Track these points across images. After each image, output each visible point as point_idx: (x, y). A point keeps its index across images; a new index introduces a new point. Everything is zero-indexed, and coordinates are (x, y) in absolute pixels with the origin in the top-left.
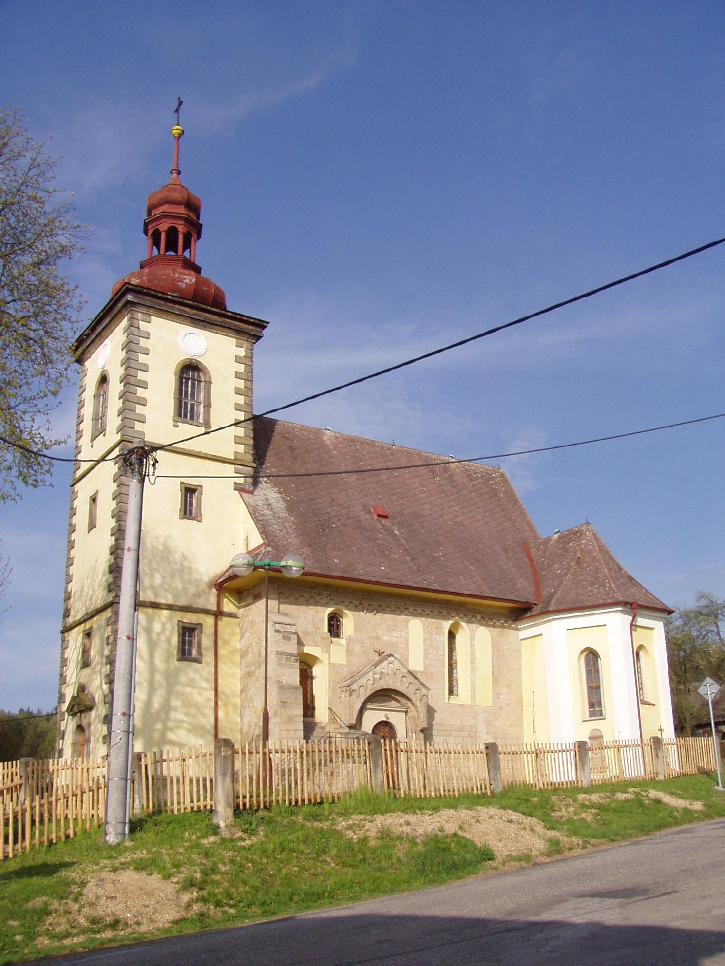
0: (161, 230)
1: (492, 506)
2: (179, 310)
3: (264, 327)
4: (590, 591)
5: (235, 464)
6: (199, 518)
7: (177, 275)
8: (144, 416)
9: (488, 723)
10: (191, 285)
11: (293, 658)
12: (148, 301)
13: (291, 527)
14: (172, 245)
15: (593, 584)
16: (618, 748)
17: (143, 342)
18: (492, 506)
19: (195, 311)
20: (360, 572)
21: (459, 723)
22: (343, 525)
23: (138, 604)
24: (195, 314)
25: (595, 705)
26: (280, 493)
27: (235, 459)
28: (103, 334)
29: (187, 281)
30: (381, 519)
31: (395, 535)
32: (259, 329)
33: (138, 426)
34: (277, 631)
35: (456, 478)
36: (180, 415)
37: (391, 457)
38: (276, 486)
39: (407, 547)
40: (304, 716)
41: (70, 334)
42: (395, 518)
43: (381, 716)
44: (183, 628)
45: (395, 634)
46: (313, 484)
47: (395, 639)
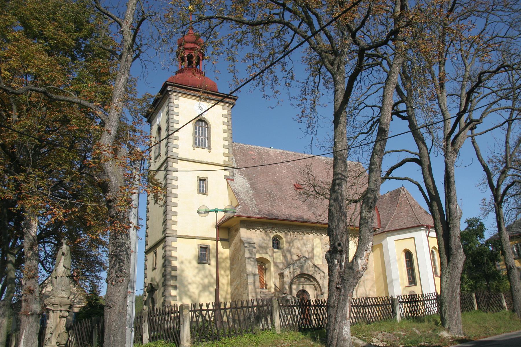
3: (236, 100)
8: (178, 145)
12: (178, 89)
14: (190, 63)
17: (176, 110)
23: (460, 96)
33: (175, 150)
41: (291, 338)
44: (201, 247)
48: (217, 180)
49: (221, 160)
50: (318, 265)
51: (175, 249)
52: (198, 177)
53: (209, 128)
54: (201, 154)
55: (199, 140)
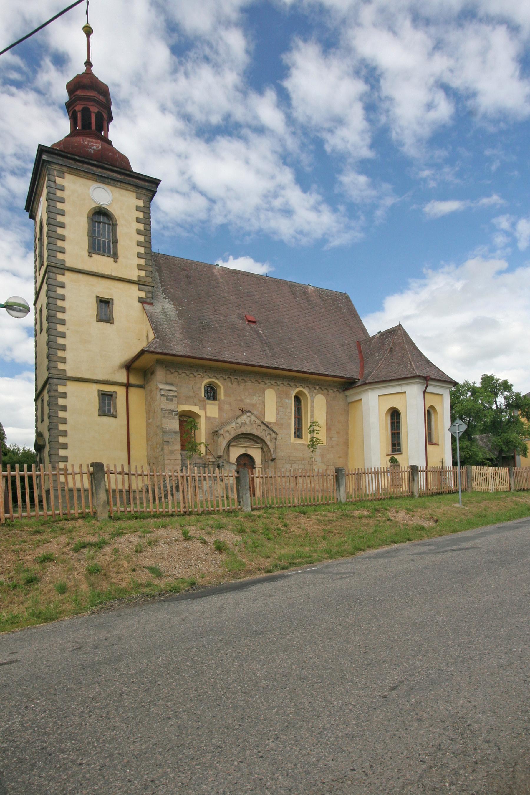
0: (77, 110)
1: (337, 317)
2: (87, 168)
4: (396, 370)
5: (138, 284)
6: (112, 321)
7: (86, 143)
8: (64, 248)
9: (322, 456)
10: (98, 151)
11: (173, 413)
12: (60, 160)
13: (178, 327)
15: (399, 364)
16: (377, 473)
18: (337, 317)
19: (100, 170)
20: (227, 356)
21: (301, 455)
22: (220, 327)
24: (100, 172)
25: (396, 444)
26: (175, 305)
27: (139, 281)
28: (38, 192)
29: (95, 147)
30: (250, 324)
31: (260, 334)
32: (154, 186)
34: (162, 395)
35: (312, 299)
36: (94, 249)
37: (264, 284)
38: (172, 300)
39: (267, 341)
40: (182, 449)
42: (262, 323)
43: (242, 451)
44: (102, 394)
45: (255, 398)
46: (202, 300)
47: (255, 402)
48: (127, 301)
49: (134, 274)
50: (270, 423)
51: (64, 395)
52: (97, 297)
53: (115, 226)
54: (101, 263)
55: (99, 244)
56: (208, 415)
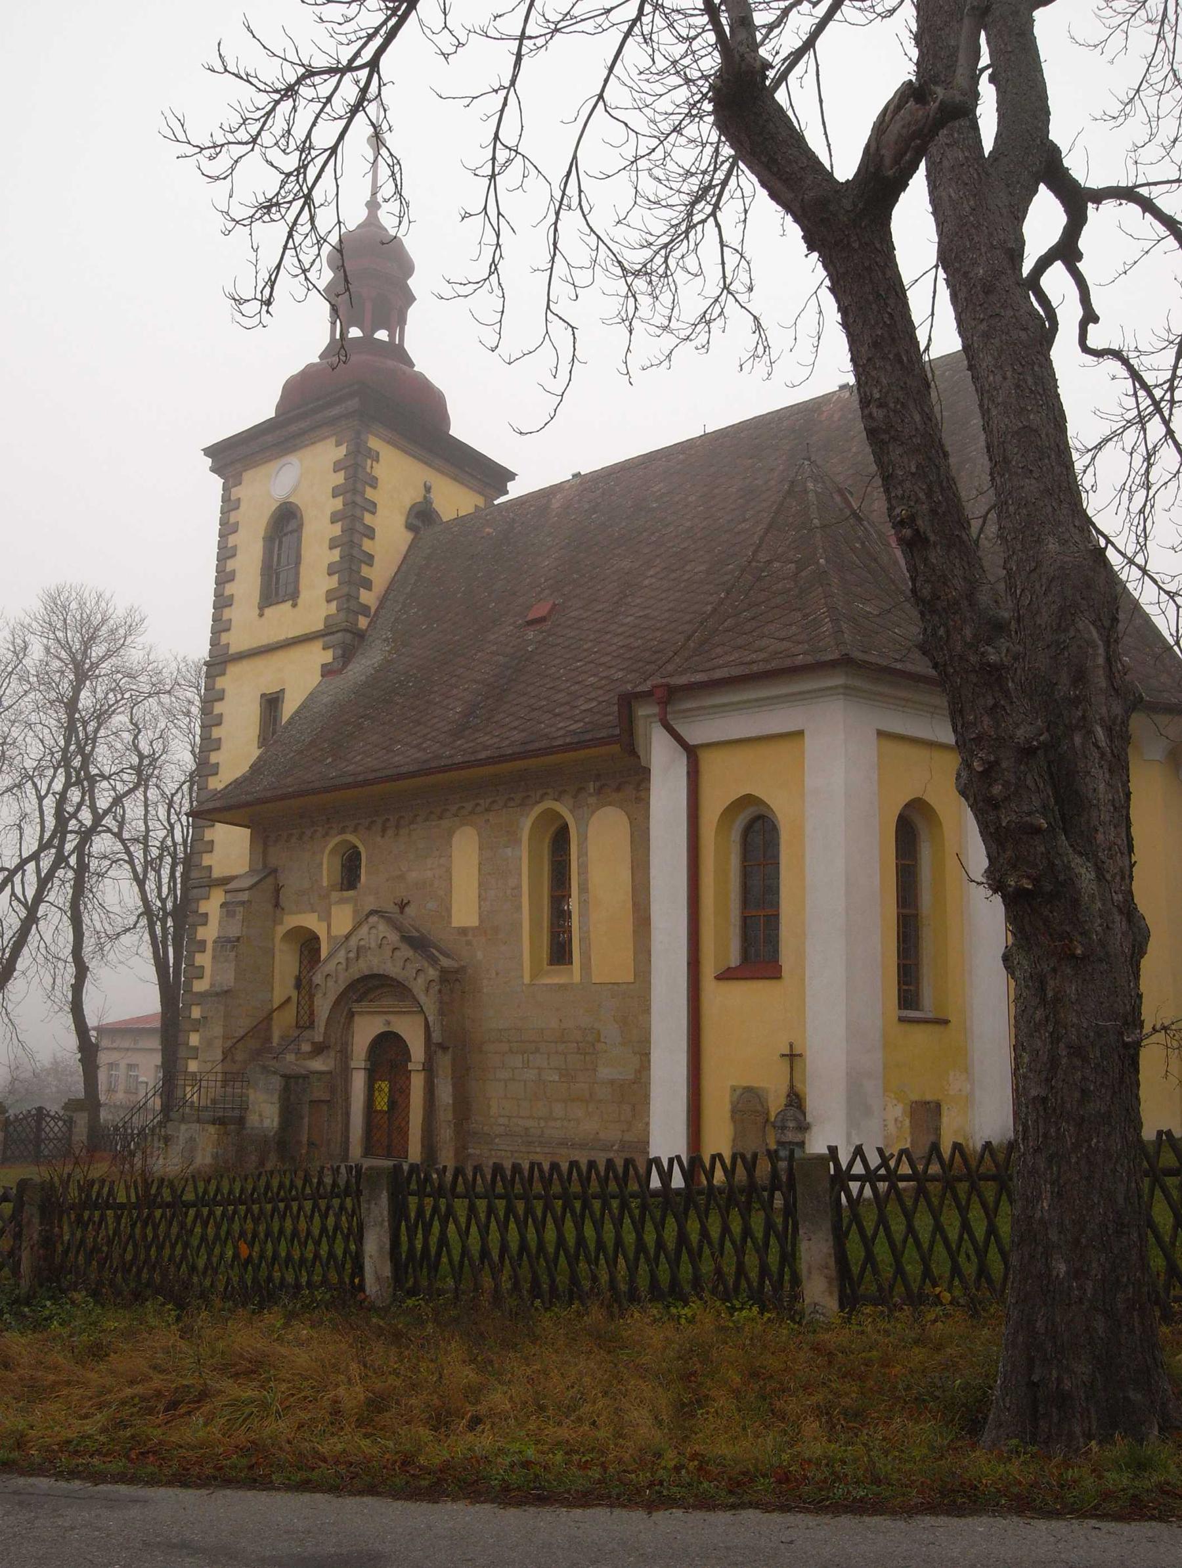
56: (334, 932)
